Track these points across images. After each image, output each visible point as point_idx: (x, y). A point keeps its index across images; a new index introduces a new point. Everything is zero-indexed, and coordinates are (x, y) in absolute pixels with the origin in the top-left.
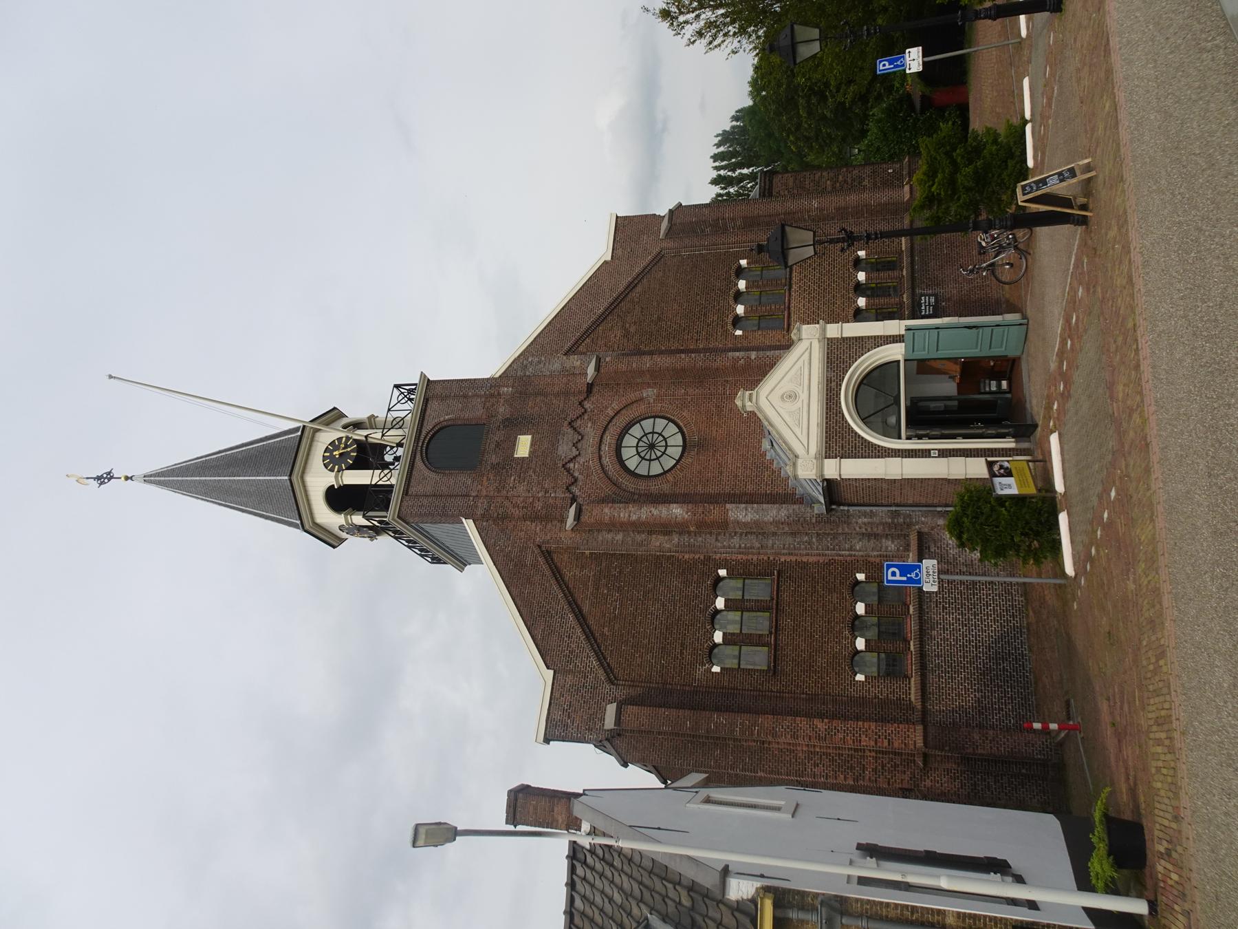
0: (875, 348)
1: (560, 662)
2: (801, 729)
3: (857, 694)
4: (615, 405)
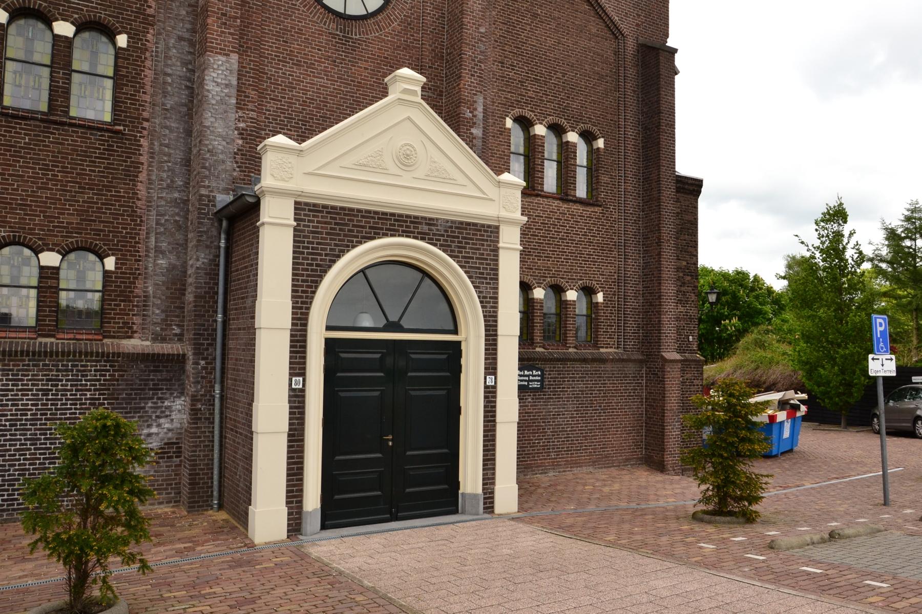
0: (479, 297)
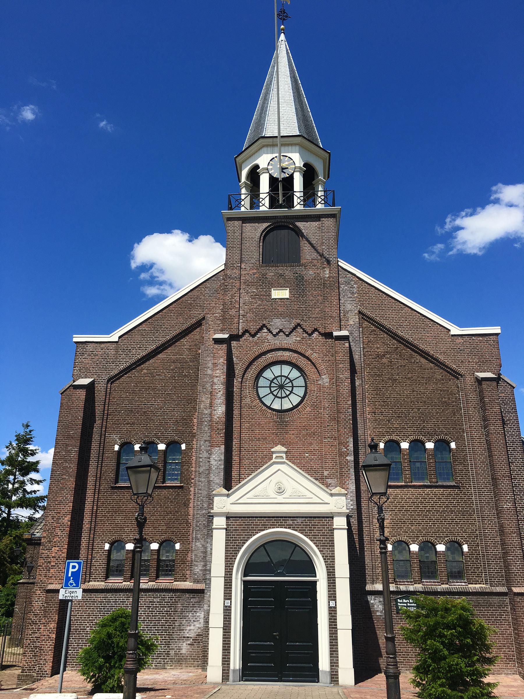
0: (323, 557)
1: (124, 344)
2: (64, 507)
3: (96, 544)
4: (314, 356)
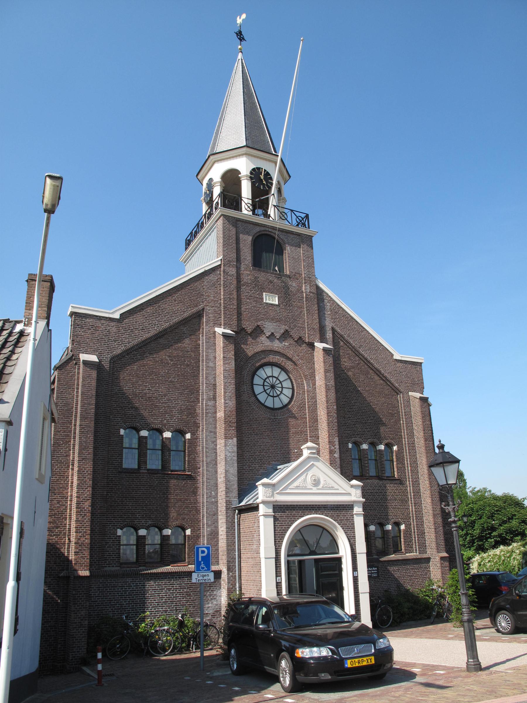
2: (84, 491)
